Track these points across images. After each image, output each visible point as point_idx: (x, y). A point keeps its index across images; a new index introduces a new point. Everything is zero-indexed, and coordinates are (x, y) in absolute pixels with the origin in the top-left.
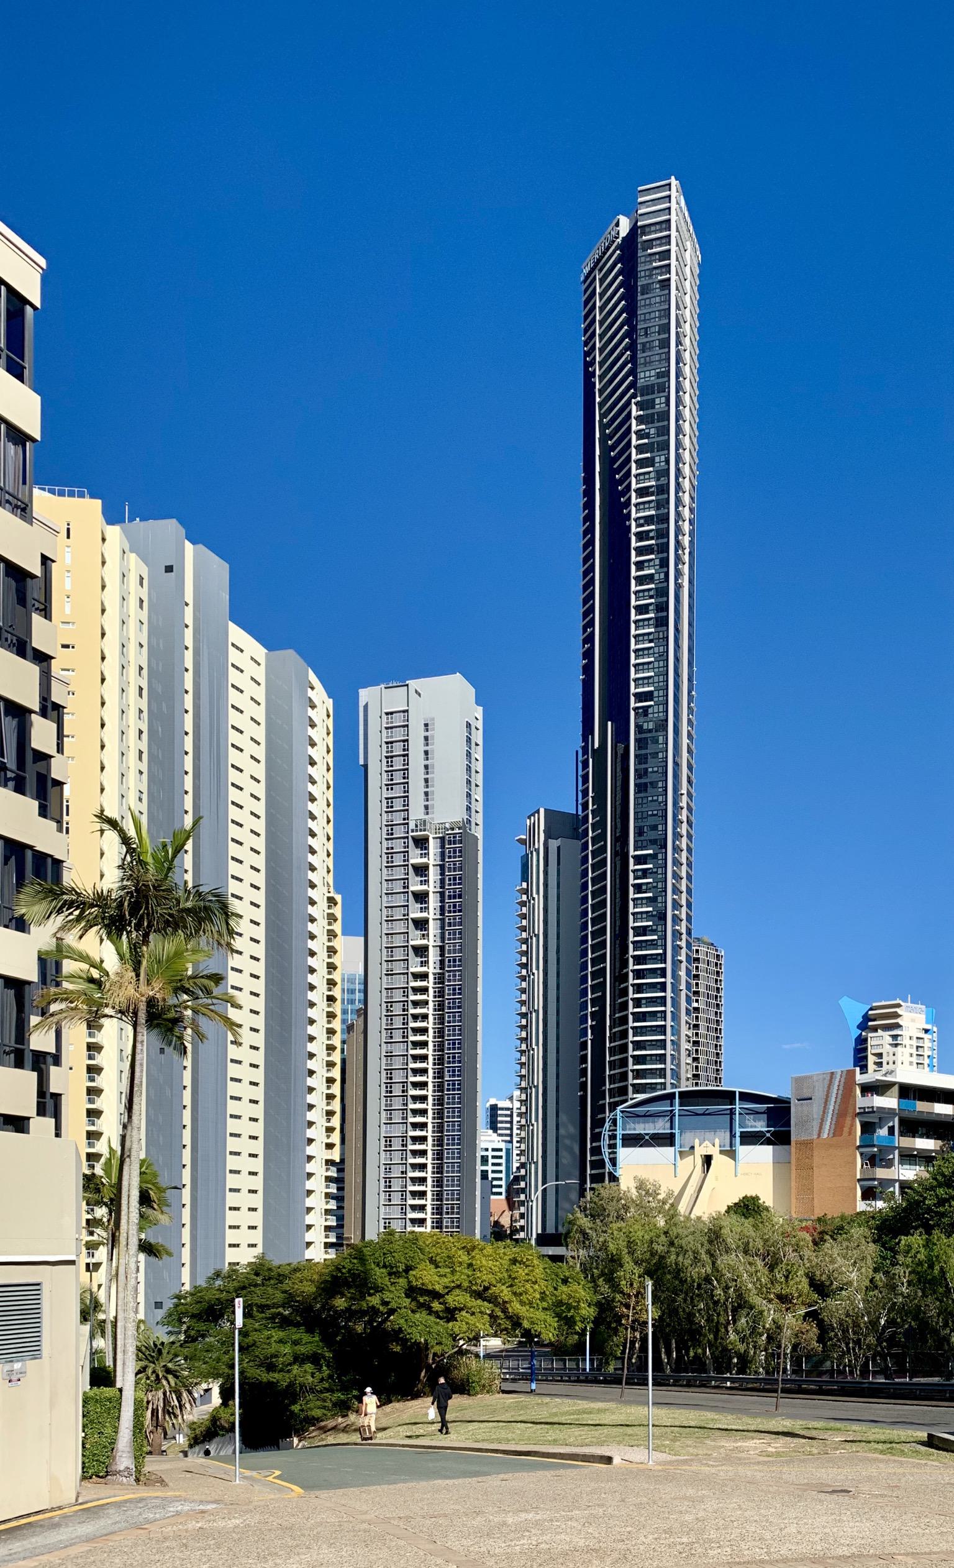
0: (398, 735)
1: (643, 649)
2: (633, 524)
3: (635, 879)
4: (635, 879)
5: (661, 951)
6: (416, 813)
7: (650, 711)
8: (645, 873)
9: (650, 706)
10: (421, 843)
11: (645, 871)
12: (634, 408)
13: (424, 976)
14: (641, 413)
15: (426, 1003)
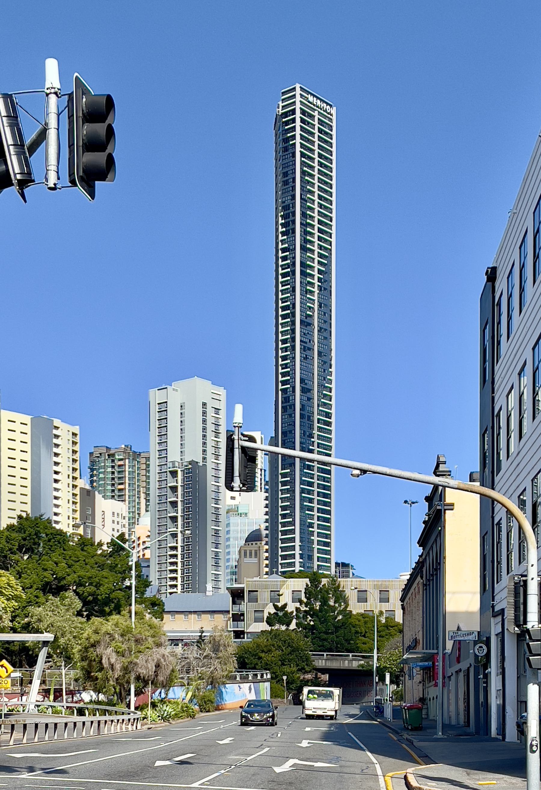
6: (174, 455)
7: (288, 390)
9: (288, 388)
10: (174, 474)
11: (286, 364)
13: (175, 548)
14: (284, 229)
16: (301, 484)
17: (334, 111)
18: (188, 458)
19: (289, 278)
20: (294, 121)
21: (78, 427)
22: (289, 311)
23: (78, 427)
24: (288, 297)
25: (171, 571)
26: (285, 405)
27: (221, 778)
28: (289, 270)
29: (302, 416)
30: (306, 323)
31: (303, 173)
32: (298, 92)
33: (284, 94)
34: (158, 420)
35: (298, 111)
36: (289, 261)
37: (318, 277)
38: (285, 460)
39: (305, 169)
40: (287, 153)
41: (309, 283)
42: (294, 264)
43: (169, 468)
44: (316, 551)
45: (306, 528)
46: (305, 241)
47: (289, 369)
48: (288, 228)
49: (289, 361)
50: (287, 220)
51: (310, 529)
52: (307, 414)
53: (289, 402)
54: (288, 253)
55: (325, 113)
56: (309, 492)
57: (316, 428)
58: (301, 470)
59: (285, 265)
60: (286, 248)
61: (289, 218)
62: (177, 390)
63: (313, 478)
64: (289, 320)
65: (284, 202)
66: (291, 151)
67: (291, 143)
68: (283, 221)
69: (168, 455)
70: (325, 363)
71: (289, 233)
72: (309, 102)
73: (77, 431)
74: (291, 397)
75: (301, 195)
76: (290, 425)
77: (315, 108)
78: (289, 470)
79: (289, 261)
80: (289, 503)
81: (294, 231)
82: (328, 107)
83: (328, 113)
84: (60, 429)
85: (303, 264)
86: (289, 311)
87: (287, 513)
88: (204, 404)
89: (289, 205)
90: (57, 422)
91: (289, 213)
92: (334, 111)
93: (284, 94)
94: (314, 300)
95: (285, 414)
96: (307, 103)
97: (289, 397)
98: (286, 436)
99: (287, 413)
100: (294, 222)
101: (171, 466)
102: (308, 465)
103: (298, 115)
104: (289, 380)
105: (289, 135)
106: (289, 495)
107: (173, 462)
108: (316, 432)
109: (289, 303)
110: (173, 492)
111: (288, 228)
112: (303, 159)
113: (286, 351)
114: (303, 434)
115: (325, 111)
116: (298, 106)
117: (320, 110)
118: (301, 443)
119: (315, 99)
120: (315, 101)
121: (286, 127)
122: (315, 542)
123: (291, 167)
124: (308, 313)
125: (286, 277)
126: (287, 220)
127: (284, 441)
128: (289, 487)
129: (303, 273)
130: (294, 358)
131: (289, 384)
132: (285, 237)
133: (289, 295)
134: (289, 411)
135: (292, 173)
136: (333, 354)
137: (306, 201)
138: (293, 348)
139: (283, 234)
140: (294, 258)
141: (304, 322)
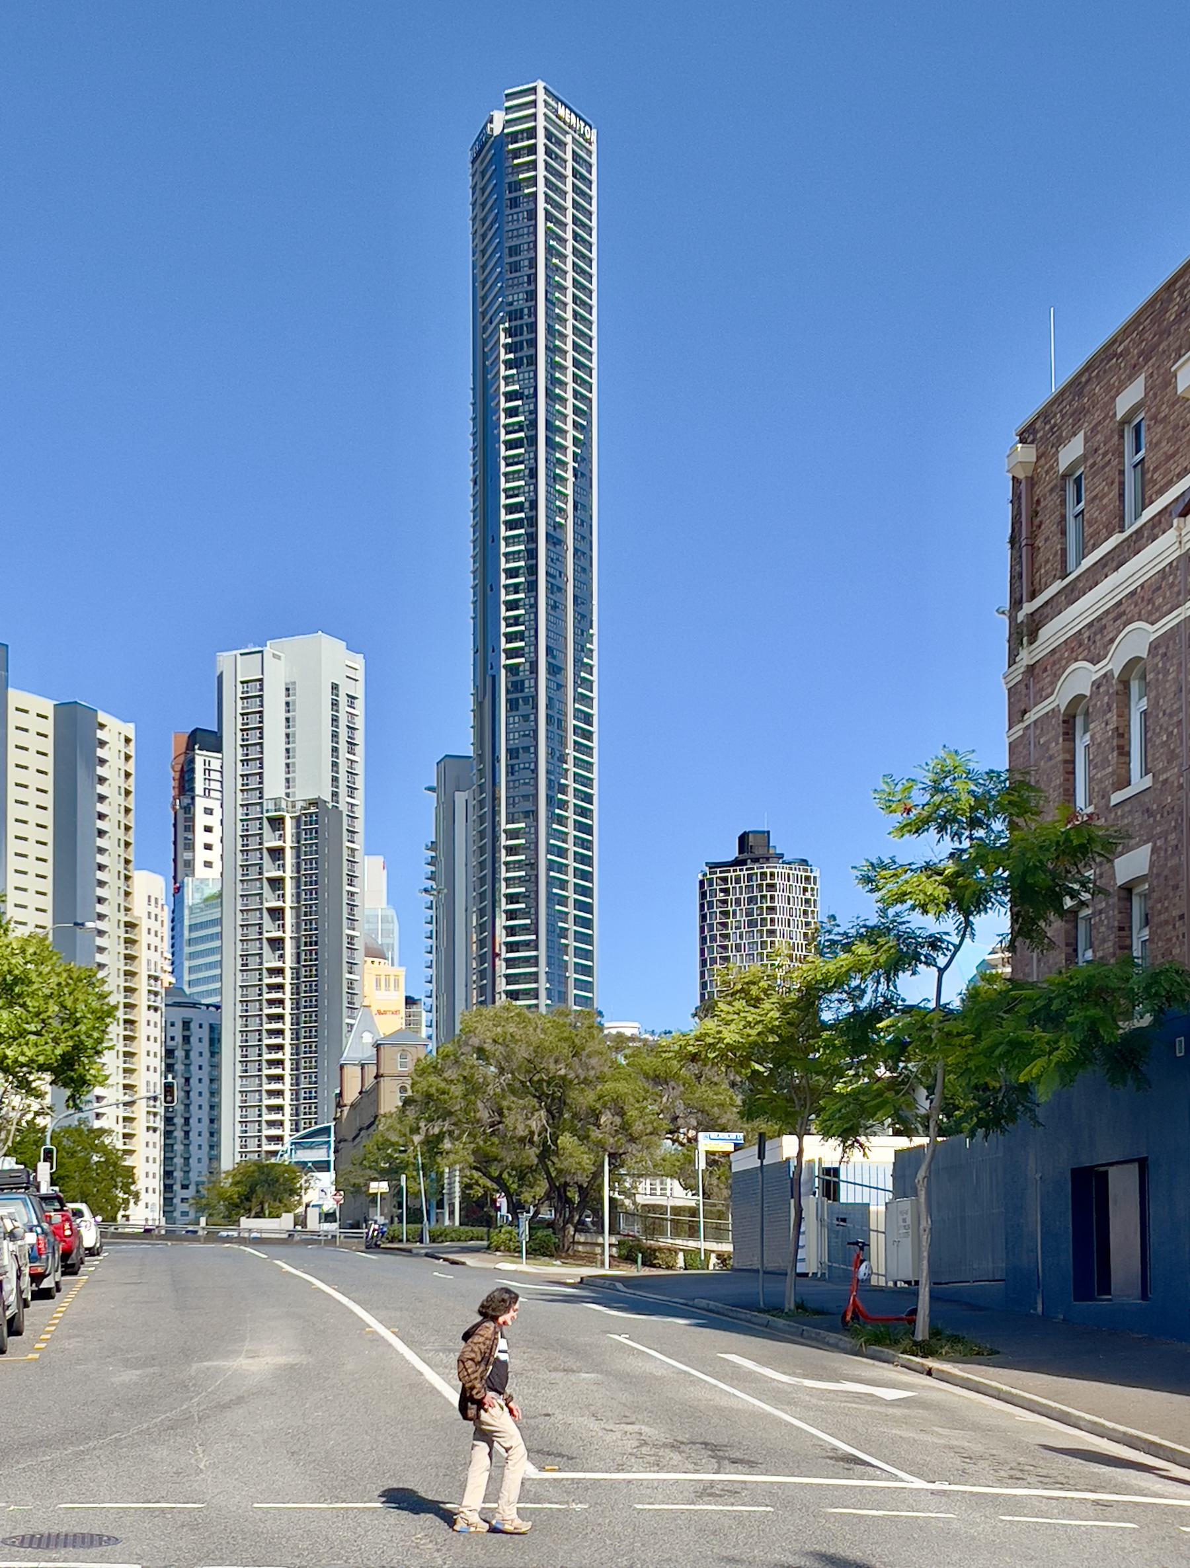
0: (253, 768)
1: (514, 553)
2: (503, 431)
3: (507, 626)
4: (507, 626)
5: (534, 937)
6: (274, 787)
7: (521, 668)
8: (516, 621)
9: (519, 664)
10: (277, 823)
11: (516, 618)
12: (502, 335)
13: (280, 971)
14: (511, 356)
15: (281, 1123)
16: (548, 852)
17: (593, 135)
18: (303, 793)
19: (522, 450)
20: (532, 150)
21: (132, 725)
22: (522, 515)
23: (132, 725)
24: (519, 488)
25: (271, 1018)
26: (514, 696)
27: (1095, 1529)
28: (522, 434)
29: (549, 718)
30: (554, 541)
31: (549, 249)
32: (541, 96)
33: (509, 97)
34: (242, 714)
35: (541, 133)
36: (522, 418)
37: (574, 452)
38: (514, 804)
39: (552, 242)
40: (517, 210)
41: (559, 461)
42: (534, 424)
43: (267, 811)
44: (571, 983)
45: (556, 939)
46: (553, 381)
47: (522, 628)
48: (519, 355)
49: (522, 612)
50: (518, 339)
51: (563, 941)
52: (557, 716)
53: (522, 691)
54: (519, 403)
55: (581, 140)
56: (562, 868)
57: (571, 744)
58: (548, 826)
59: (513, 424)
60: (515, 392)
61: (521, 334)
62: (279, 658)
63: (565, 841)
64: (522, 531)
65: (511, 304)
66: (525, 206)
67: (527, 191)
68: (509, 340)
69: (266, 786)
70: (583, 616)
71: (522, 364)
72: (558, 117)
73: (132, 736)
74: (527, 682)
75: (546, 292)
76: (525, 735)
77: (567, 128)
78: (523, 825)
79: (522, 418)
80: (523, 890)
81: (533, 361)
82: (587, 128)
83: (586, 140)
84: (106, 729)
85: (549, 425)
86: (522, 515)
87: (520, 909)
88: (335, 687)
89: (522, 310)
90: (102, 717)
91: (522, 326)
92: (593, 135)
93: (509, 97)
94: (566, 496)
95: (514, 713)
96: (554, 117)
97: (523, 682)
98: (517, 758)
99: (518, 713)
100: (533, 343)
101: (271, 806)
102: (559, 815)
103: (541, 140)
104: (522, 648)
105: (521, 176)
106: (523, 873)
107: (276, 800)
108: (570, 750)
109: (522, 499)
110: (274, 859)
111: (519, 355)
112: (549, 224)
113: (516, 592)
114: (551, 753)
115: (583, 136)
116: (541, 123)
117: (577, 136)
118: (548, 772)
119: (568, 111)
120: (568, 116)
121: (516, 162)
122: (571, 967)
123: (526, 239)
124: (558, 519)
125: (517, 448)
126: (518, 339)
127: (512, 766)
128: (523, 857)
129: (549, 442)
130: (535, 606)
131: (522, 656)
132: (514, 371)
133: (522, 483)
134: (524, 709)
135: (529, 249)
136: (595, 602)
137: (554, 304)
138: (532, 587)
139: (509, 364)
140: (535, 412)
141: (553, 537)
